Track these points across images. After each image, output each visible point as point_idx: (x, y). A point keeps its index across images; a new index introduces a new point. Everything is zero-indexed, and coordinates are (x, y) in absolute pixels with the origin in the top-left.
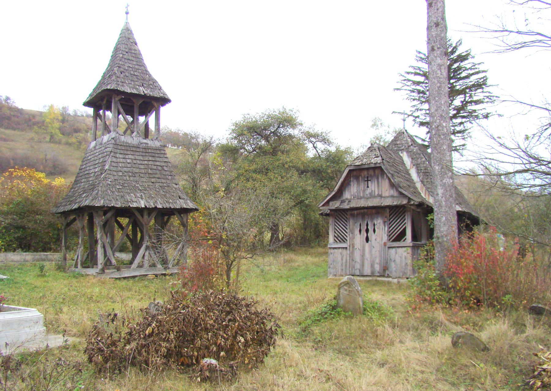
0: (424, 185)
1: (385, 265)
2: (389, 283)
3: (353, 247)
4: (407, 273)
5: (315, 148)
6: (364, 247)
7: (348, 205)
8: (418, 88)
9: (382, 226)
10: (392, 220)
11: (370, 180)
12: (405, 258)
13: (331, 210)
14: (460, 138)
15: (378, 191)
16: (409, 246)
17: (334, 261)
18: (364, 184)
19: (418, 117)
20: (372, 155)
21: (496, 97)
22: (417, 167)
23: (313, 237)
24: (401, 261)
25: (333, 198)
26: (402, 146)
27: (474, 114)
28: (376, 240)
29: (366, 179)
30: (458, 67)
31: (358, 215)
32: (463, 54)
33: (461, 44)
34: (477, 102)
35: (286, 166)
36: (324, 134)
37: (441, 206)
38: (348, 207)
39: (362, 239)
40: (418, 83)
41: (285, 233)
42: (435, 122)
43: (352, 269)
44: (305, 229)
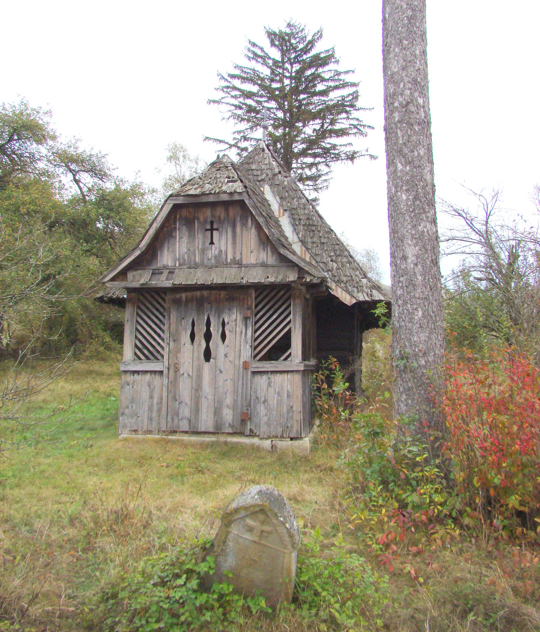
0: (307, 249)
1: (245, 410)
2: (257, 449)
3: (177, 370)
4: (292, 427)
5: (77, 182)
6: (200, 370)
7: (167, 279)
8: (249, 102)
9: (240, 326)
10: (261, 313)
11: (217, 229)
12: (288, 396)
13: (130, 290)
14: (311, 187)
15: (234, 253)
16: (297, 371)
17: (133, 401)
18: (204, 236)
19: (245, 149)
20: (223, 176)
21: (369, 127)
22: (292, 214)
23: (64, 343)
24: (279, 403)
25: (135, 265)
26: (262, 174)
27: (332, 151)
28: (226, 356)
29: (209, 227)
30: (312, 74)
31: (188, 301)
32: (322, 55)
33: (321, 37)
34: (342, 133)
35: (23, 210)
36: (94, 159)
37: (414, 285)
38: (168, 284)
39: (196, 354)
40: (249, 95)
41: (13, 333)
42: (402, 95)
43: (173, 419)
44: (51, 329)
